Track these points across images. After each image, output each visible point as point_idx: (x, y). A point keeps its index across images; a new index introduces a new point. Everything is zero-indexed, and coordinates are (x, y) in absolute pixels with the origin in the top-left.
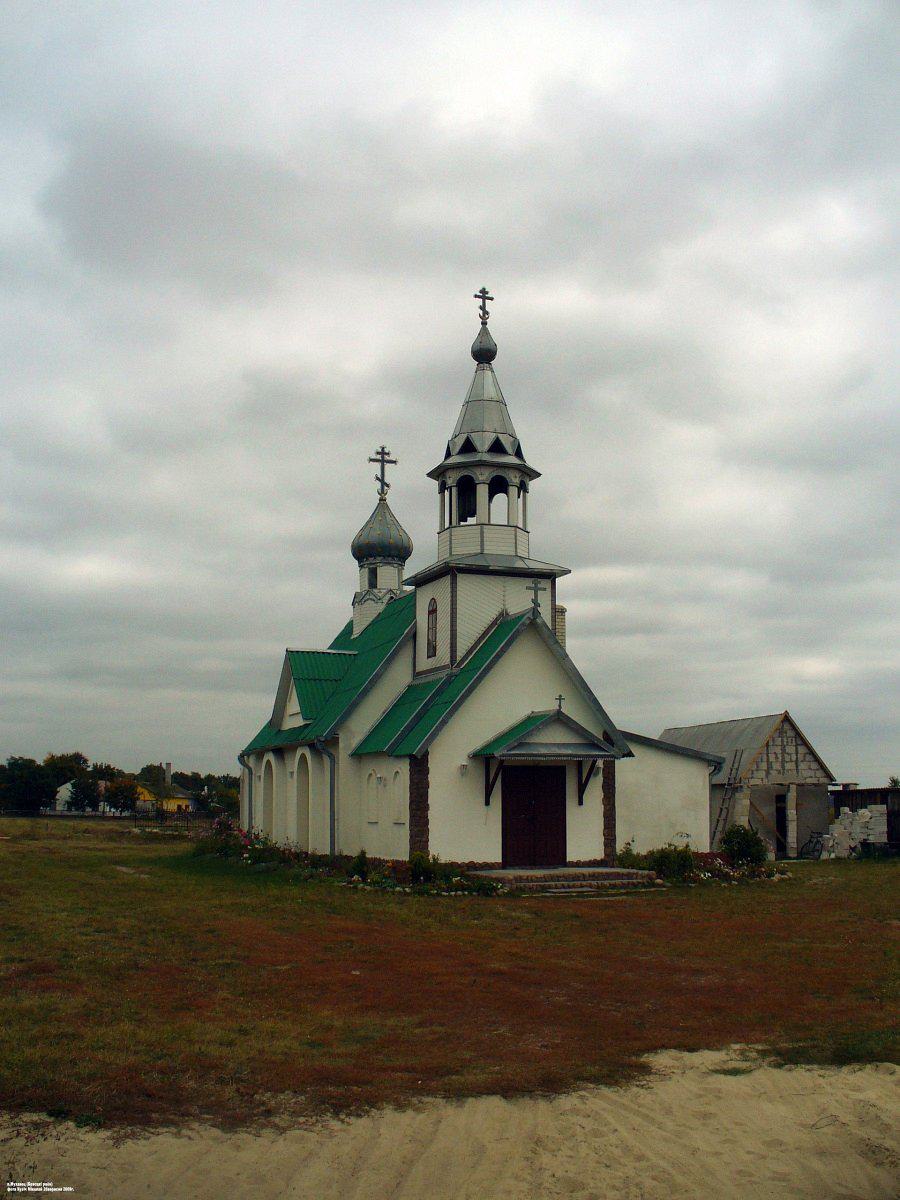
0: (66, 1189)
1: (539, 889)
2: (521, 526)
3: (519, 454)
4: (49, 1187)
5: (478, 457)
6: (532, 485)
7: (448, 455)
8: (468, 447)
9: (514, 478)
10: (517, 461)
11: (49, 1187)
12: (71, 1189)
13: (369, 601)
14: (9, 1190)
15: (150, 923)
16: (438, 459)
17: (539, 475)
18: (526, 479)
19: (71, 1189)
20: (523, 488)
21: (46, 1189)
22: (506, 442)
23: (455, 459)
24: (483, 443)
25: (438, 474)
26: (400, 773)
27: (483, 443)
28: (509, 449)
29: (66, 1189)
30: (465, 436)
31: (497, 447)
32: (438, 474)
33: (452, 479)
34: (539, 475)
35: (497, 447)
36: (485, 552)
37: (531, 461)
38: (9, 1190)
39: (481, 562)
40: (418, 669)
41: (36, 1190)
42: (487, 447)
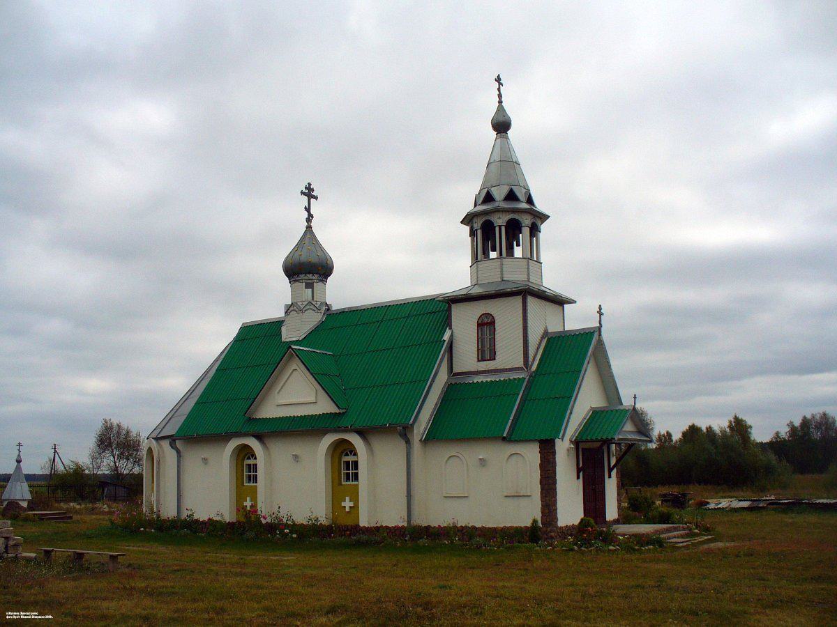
0: (47, 617)
1: (681, 529)
2: (535, 259)
3: (530, 200)
4: (35, 615)
5: (495, 205)
6: (545, 227)
7: (475, 205)
8: (489, 198)
9: (526, 221)
10: (524, 206)
11: (35, 615)
12: (51, 617)
13: (308, 311)
14: (7, 617)
15: (461, 596)
16: (469, 207)
17: (548, 217)
18: (538, 222)
19: (51, 617)
20: (534, 230)
21: (33, 617)
22: (520, 194)
23: (480, 208)
24: (499, 194)
25: (468, 220)
26: (531, 454)
27: (499, 194)
28: (522, 197)
29: (47, 617)
30: (486, 189)
31: (511, 196)
32: (468, 220)
33: (478, 224)
34: (548, 217)
35: (511, 196)
36: (504, 279)
37: (540, 206)
38: (7, 617)
39: (501, 287)
40: (455, 370)
41: (27, 617)
42: (503, 196)
